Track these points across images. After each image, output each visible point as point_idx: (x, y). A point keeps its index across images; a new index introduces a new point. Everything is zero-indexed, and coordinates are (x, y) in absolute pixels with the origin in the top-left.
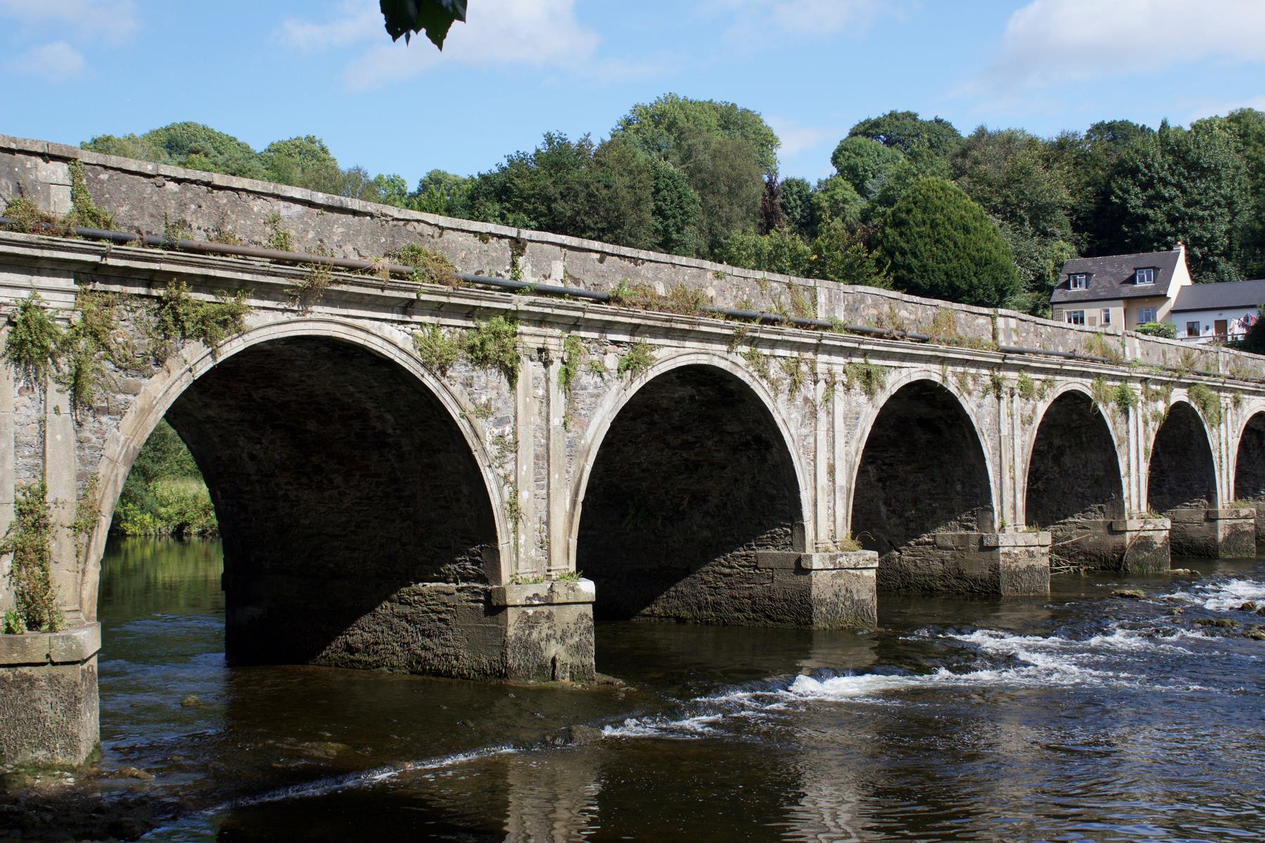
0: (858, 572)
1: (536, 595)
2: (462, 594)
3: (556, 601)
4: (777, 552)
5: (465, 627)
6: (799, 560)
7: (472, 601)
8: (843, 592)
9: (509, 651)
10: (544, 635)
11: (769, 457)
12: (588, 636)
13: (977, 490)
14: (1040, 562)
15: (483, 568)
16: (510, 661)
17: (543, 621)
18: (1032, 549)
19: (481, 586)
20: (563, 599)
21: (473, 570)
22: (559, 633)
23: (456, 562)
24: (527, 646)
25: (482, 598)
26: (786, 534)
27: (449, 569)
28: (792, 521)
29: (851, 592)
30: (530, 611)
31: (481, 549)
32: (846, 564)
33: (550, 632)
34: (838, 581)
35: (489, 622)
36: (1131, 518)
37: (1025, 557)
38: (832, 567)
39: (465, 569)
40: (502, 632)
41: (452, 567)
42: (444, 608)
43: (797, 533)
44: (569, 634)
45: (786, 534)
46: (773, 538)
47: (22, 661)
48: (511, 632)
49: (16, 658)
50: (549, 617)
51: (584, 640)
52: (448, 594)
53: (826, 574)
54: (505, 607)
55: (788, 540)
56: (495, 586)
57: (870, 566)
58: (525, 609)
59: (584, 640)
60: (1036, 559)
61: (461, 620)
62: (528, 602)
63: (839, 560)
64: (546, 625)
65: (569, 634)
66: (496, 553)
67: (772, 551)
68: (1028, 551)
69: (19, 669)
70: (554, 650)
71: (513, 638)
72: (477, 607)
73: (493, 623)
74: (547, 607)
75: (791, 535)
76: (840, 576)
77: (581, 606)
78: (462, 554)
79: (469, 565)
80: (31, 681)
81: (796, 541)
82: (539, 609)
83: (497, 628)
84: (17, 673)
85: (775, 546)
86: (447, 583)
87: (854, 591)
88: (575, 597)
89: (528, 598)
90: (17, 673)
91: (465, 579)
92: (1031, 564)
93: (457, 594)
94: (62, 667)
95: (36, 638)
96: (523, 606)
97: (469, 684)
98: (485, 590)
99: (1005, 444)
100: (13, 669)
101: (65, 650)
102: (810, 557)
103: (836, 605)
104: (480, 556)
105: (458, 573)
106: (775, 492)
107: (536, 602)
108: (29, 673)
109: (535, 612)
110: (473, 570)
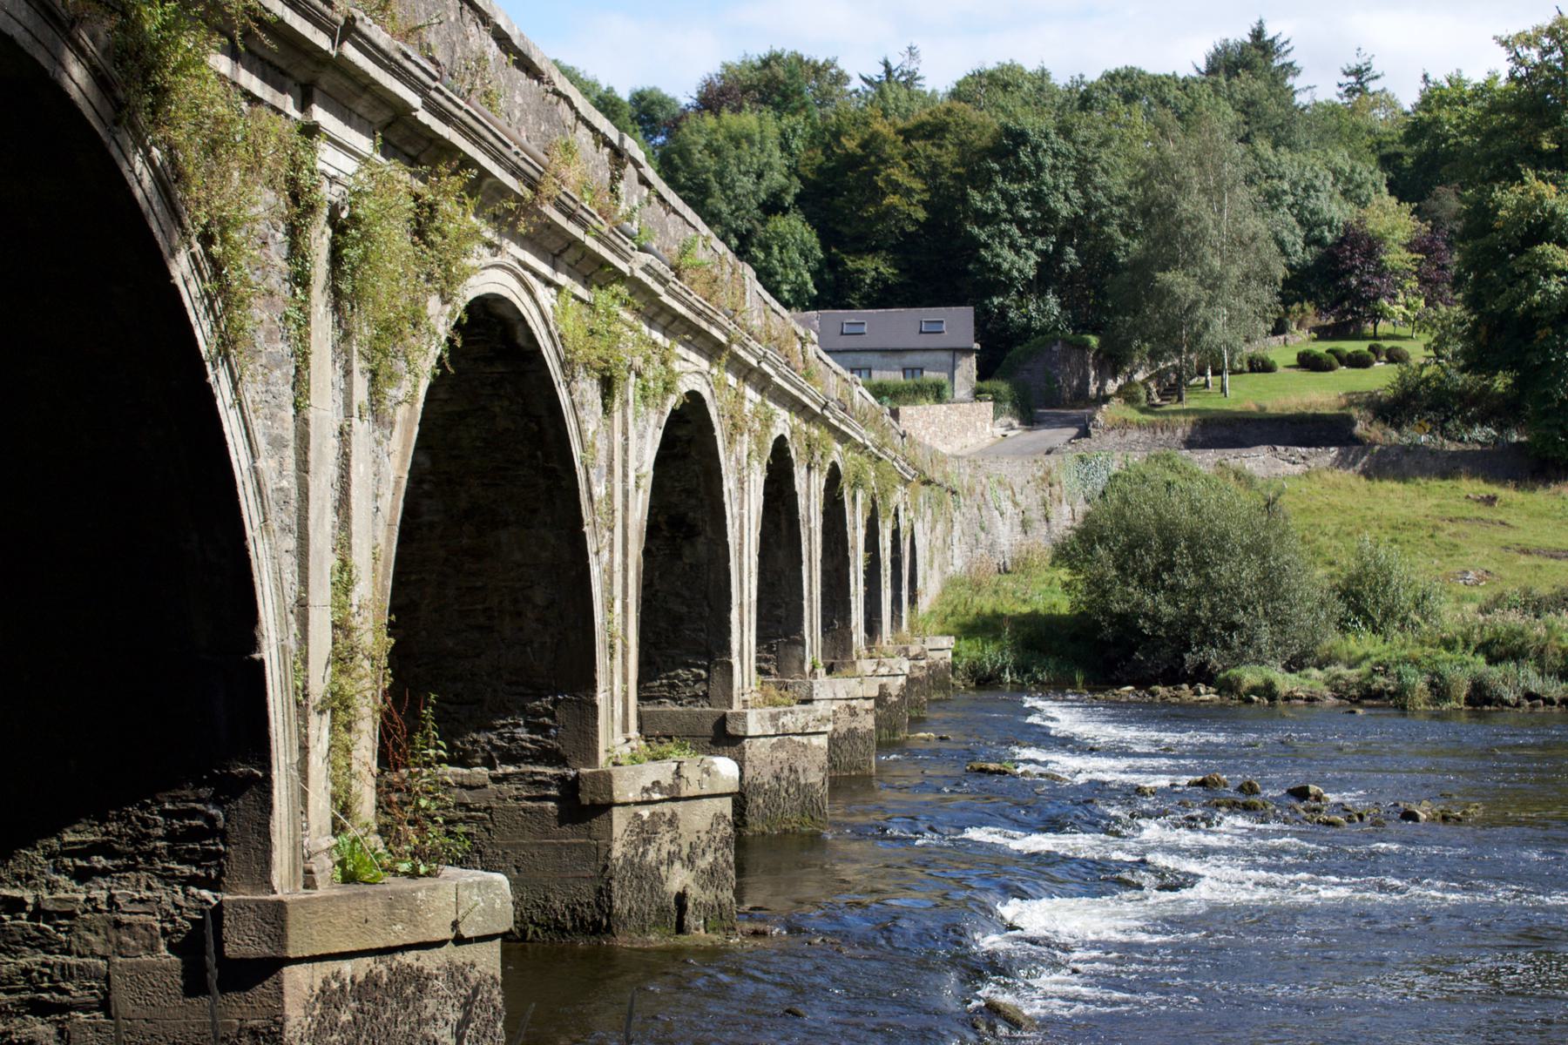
0: (804, 740)
1: (656, 783)
2: (505, 786)
3: (684, 793)
4: (677, 708)
5: (509, 846)
6: (722, 721)
7: (528, 799)
8: (786, 772)
9: (615, 884)
10: (664, 854)
11: (687, 551)
12: (727, 851)
13: (781, 612)
14: (863, 723)
15: (556, 738)
16: (617, 904)
17: (664, 827)
18: (854, 703)
19: (550, 771)
20: (693, 790)
21: (533, 741)
22: (686, 851)
23: (492, 728)
24: (646, 877)
25: (553, 792)
26: (698, 678)
27: (475, 742)
28: (709, 656)
29: (796, 772)
30: (645, 812)
31: (555, 703)
32: (791, 728)
33: (673, 848)
34: (778, 754)
35: (571, 836)
36: (859, 658)
37: (844, 716)
38: (772, 732)
39: (513, 739)
40: (601, 854)
41: (482, 738)
42: (462, 814)
43: (717, 677)
44: (699, 851)
45: (698, 678)
46: (672, 686)
47: (410, 940)
48: (618, 851)
49: (400, 934)
50: (672, 822)
51: (721, 860)
52: (470, 788)
53: (763, 744)
54: (610, 805)
55: (700, 688)
56: (584, 770)
57: (822, 729)
58: (638, 809)
59: (721, 860)
60: (859, 719)
61: (502, 834)
62: (646, 797)
63: (783, 720)
64: (668, 837)
65: (699, 851)
66: (589, 710)
67: (670, 707)
68: (848, 706)
69: (399, 956)
70: (678, 879)
71: (621, 861)
72: (543, 810)
73: (579, 836)
74: (670, 804)
75: (707, 681)
76: (781, 746)
77: (716, 801)
78: (508, 712)
79: (522, 733)
80: (420, 980)
81: (716, 689)
82: (657, 808)
83: (589, 846)
84: (394, 965)
85: (675, 700)
86: (468, 766)
87: (800, 770)
88: (711, 785)
89: (646, 790)
90: (394, 965)
91: (508, 758)
92: (853, 725)
93: (491, 786)
94: (479, 945)
95: (435, 888)
96: (637, 803)
97: (524, 949)
98: (562, 779)
99: (261, 553)
100: (387, 958)
101: (483, 912)
102: (742, 717)
103: (777, 793)
104: (552, 716)
105: (495, 748)
106: (684, 609)
107: (656, 796)
108: (416, 964)
109: (653, 814)
110: (533, 741)
